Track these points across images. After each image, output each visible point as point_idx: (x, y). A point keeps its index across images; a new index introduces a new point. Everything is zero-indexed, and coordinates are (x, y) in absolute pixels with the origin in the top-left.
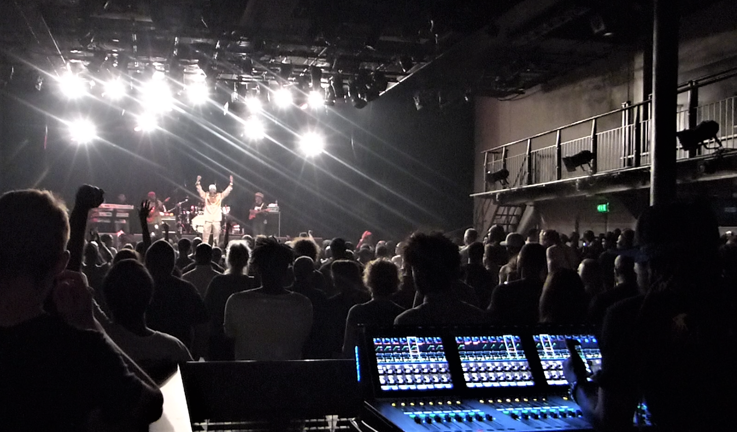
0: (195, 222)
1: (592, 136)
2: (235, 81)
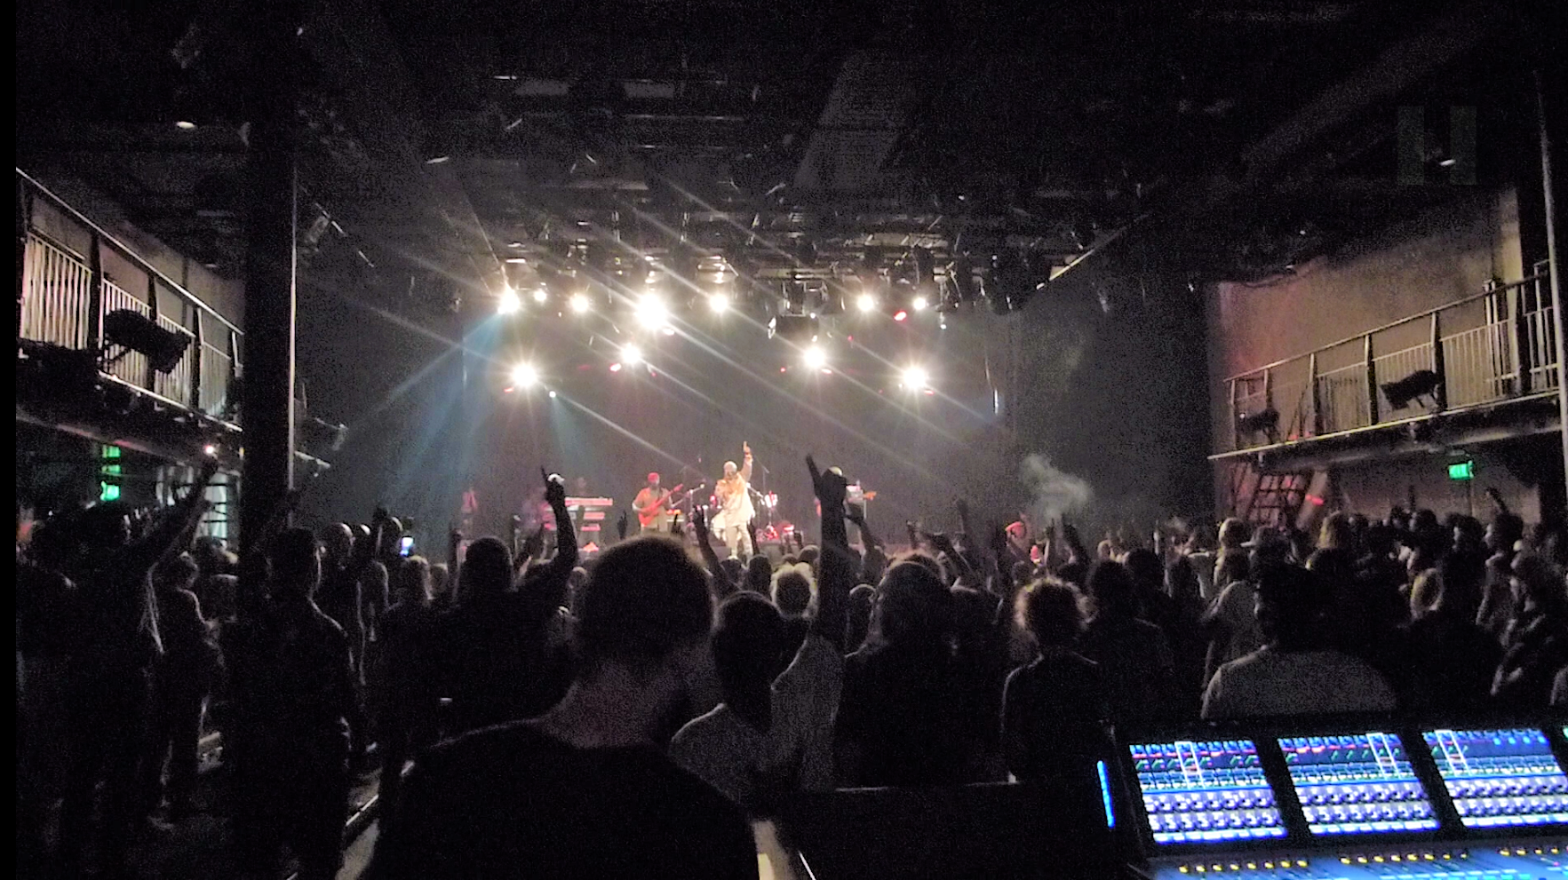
1: (1432, 343)
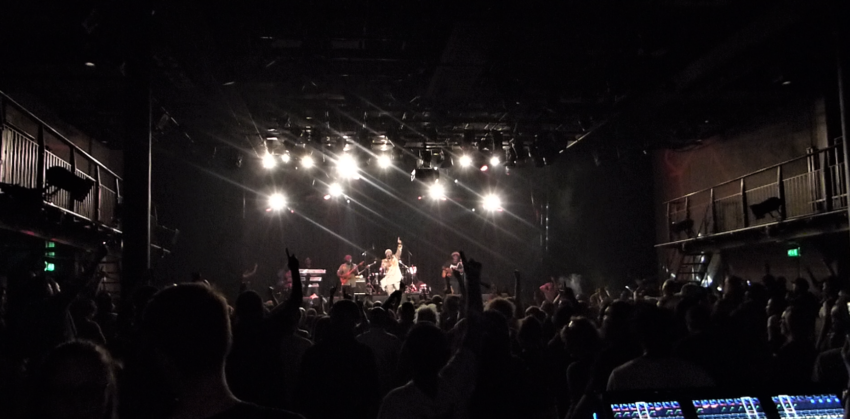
0: (384, 283)
2: (419, 148)
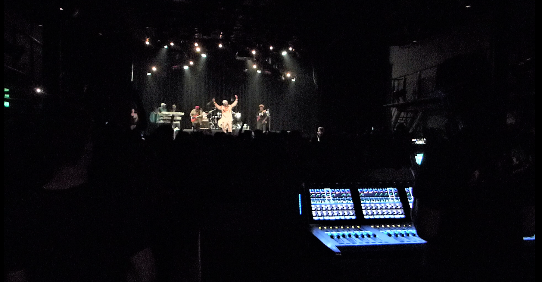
0: (220, 123)
